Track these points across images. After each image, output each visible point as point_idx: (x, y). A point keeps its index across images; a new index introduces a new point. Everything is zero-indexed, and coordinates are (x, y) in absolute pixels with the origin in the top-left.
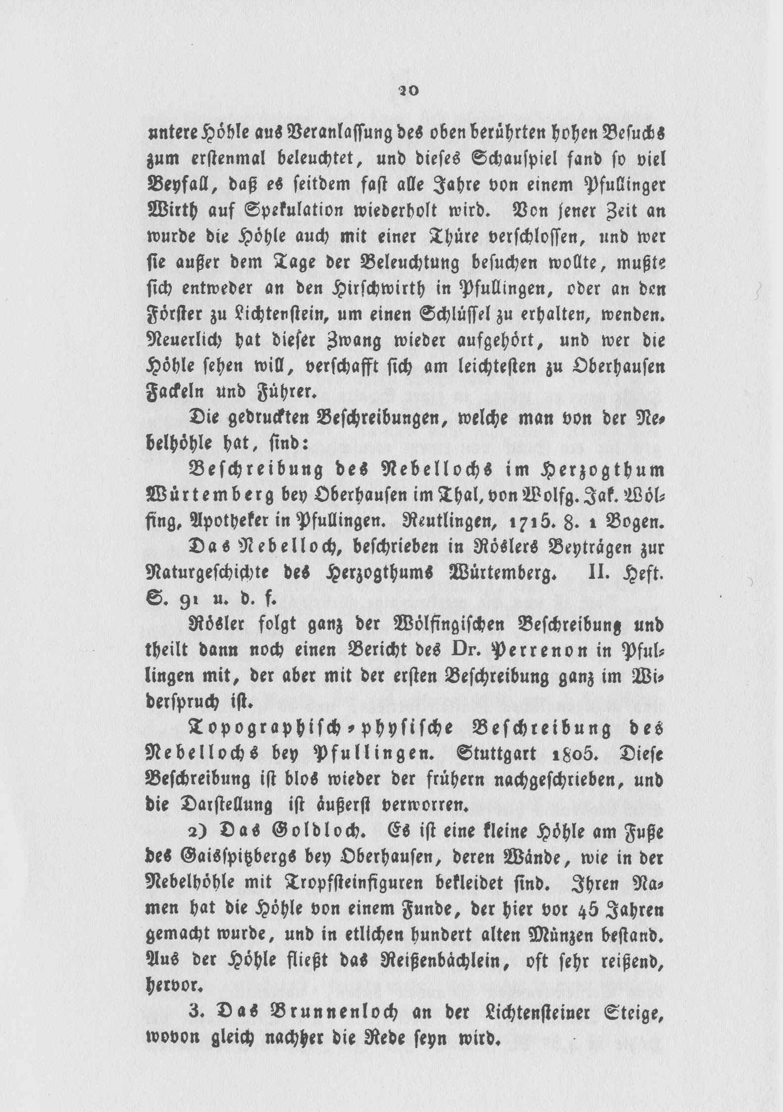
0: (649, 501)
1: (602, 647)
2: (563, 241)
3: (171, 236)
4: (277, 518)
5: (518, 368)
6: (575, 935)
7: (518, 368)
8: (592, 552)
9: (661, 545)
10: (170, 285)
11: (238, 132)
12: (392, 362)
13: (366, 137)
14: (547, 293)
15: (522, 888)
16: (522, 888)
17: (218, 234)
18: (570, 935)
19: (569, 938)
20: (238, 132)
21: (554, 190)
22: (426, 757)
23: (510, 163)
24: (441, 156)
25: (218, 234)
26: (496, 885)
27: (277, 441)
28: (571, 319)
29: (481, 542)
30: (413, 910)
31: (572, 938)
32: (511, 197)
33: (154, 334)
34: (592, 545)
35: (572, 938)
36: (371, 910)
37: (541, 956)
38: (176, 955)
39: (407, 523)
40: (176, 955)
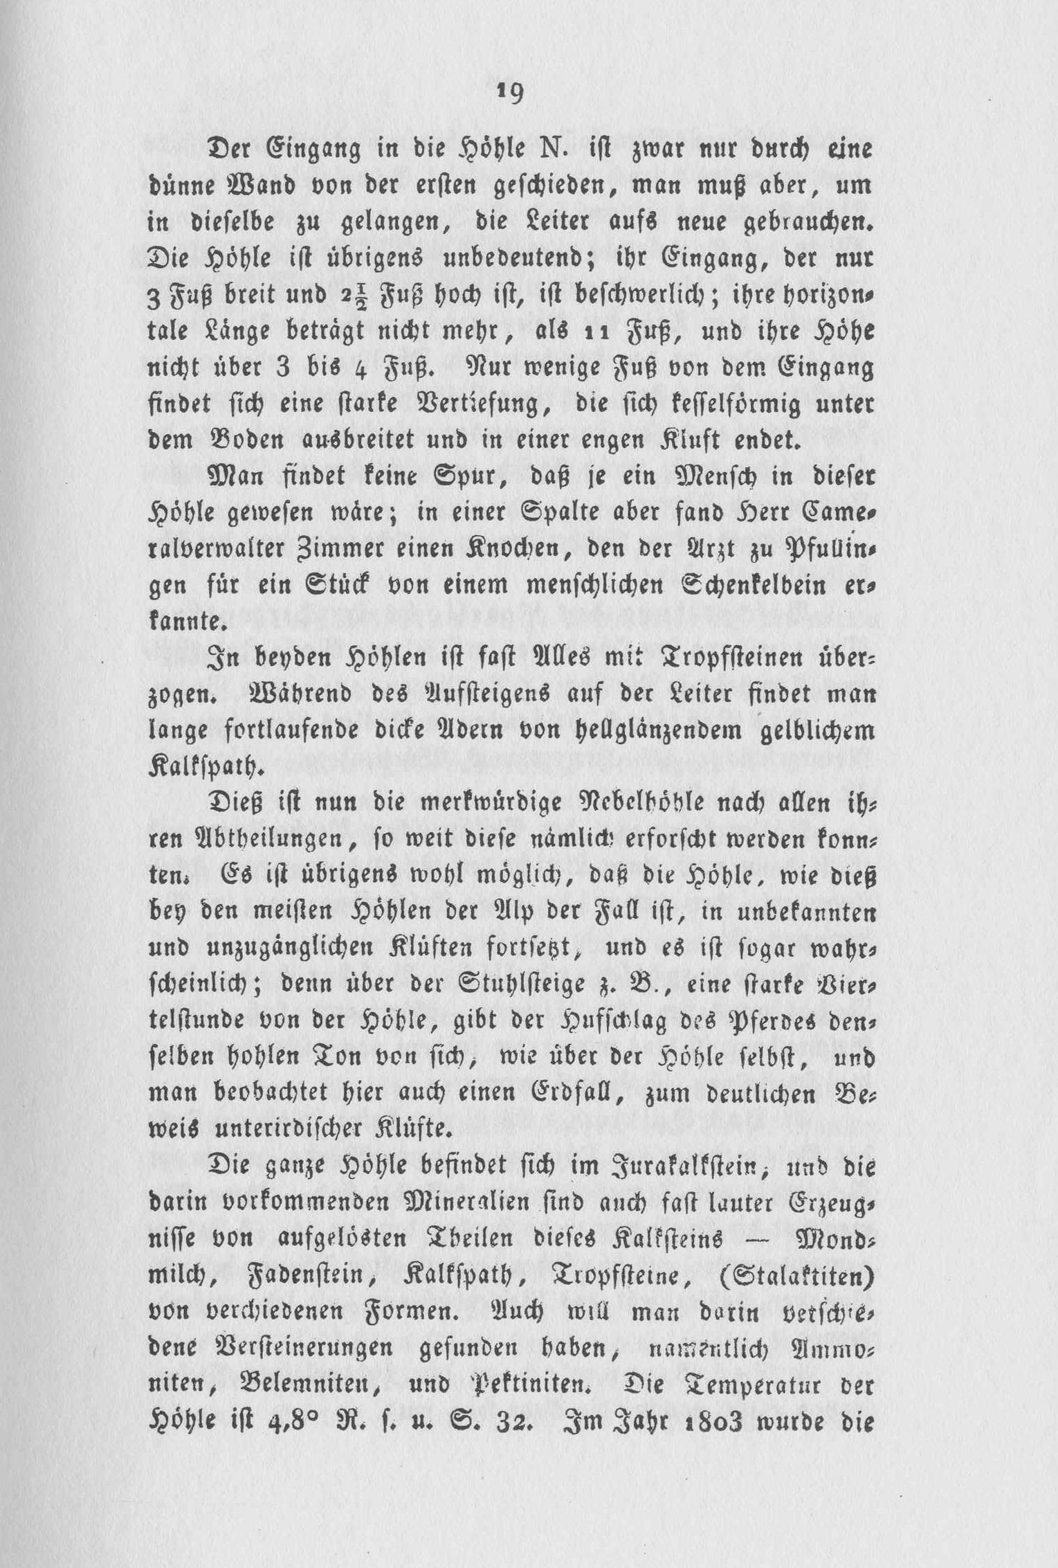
0: (190, 726)
1: (155, 217)
2: (314, 736)
3: (485, 476)
4: (574, 1162)
5: (451, 187)
6: (671, 730)
7: (451, 187)
8: (324, 337)
9: (868, 254)
10: (478, 290)
11: (510, 148)
12: (528, 1158)
13: (501, 410)
14: (371, 1391)
15: (554, 1208)
16: (554, 1208)
17: (482, 835)
18: (663, 730)
19: (662, 734)
20: (510, 148)
21: (434, 555)
22: (206, 700)
23: (618, 226)
24: (603, 290)
25: (482, 835)
26: (335, 478)
27: (553, 1198)
28: (453, 954)
29: (347, 1413)
30: (395, 295)
31: (667, 734)
32: (243, 1255)
33: (476, 360)
34: (323, 328)
35: (667, 734)
36: (484, 514)
37: (710, 433)
38: (418, 251)
39: (343, 1424)
40: (418, 251)
